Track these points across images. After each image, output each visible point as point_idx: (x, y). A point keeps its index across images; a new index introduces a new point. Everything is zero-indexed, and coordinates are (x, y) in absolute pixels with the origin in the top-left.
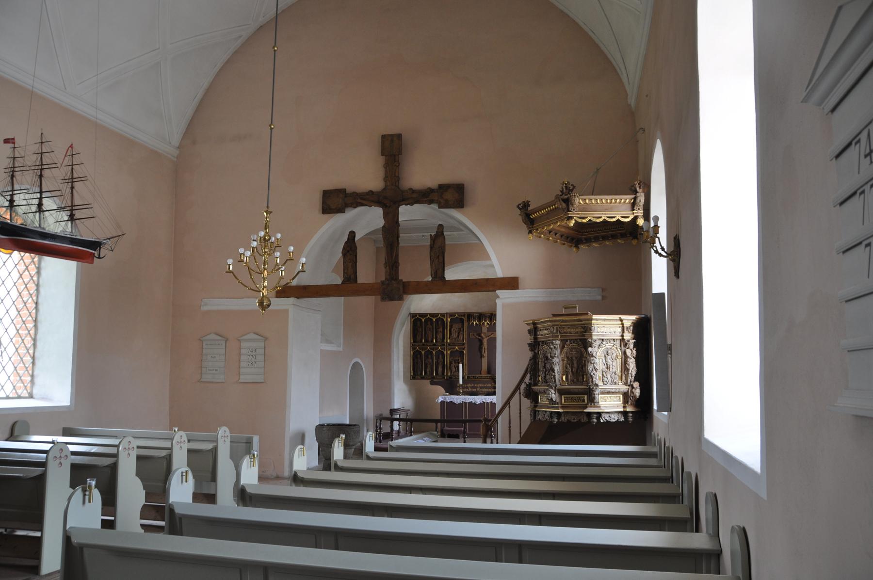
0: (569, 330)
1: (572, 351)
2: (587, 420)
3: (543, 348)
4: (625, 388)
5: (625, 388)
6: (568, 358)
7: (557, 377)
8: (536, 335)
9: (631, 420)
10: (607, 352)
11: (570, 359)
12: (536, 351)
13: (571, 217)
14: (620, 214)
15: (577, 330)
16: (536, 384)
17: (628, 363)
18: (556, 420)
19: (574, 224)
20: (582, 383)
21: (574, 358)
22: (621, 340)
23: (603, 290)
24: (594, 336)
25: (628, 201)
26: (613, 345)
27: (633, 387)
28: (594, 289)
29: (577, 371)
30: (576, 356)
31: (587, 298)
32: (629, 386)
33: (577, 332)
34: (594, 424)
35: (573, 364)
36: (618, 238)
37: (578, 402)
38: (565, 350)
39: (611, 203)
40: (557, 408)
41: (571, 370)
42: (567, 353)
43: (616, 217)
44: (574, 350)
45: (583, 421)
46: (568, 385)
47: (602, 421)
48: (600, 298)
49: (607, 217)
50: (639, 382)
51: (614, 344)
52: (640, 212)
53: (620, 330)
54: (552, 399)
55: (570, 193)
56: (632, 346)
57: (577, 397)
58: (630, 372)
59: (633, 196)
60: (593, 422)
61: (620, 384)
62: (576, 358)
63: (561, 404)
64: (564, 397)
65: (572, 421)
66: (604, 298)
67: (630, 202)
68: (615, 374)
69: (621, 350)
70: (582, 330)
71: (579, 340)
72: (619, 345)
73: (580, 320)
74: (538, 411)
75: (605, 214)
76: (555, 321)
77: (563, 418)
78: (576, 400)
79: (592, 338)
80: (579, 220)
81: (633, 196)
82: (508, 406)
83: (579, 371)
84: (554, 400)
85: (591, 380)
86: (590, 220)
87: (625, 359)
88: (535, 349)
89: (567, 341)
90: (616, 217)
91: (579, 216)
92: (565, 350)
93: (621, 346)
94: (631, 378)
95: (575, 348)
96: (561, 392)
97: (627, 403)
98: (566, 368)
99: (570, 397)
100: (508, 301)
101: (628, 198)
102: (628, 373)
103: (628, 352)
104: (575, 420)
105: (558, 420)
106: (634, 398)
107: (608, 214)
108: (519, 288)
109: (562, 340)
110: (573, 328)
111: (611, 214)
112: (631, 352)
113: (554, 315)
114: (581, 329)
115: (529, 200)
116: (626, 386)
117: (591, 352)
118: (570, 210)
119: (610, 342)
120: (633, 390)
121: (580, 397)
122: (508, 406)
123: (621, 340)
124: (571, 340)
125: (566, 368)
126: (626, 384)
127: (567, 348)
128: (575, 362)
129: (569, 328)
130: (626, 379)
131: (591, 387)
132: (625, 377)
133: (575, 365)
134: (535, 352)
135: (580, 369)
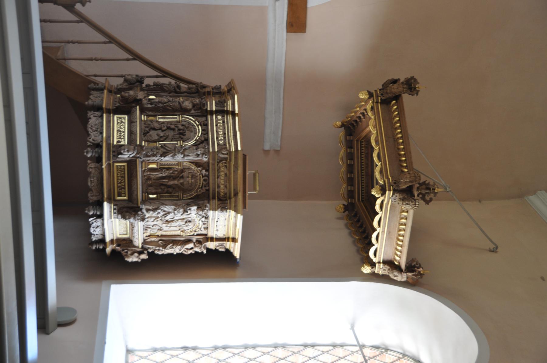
0: (222, 175)
1: (192, 177)
2: (91, 201)
3: (198, 126)
4: (138, 242)
5: (138, 242)
6: (182, 171)
7: (155, 158)
8: (215, 94)
9: (94, 247)
10: (190, 221)
11: (180, 173)
12: (193, 111)
13: (385, 193)
14: (381, 248)
15: (222, 186)
16: (142, 111)
17: (174, 247)
18: (89, 155)
19: (374, 196)
20: (146, 192)
21: (182, 181)
22: (206, 235)
23: (277, 151)
24: (213, 213)
25: (398, 258)
26: (200, 227)
27: (140, 253)
28: (279, 140)
29: (163, 185)
30: (185, 183)
31: (267, 131)
32: (142, 247)
33: (219, 187)
34: (86, 212)
35: (174, 179)
36: (348, 186)
37: (118, 187)
38: (193, 167)
39: (398, 240)
40: (108, 159)
41: (164, 175)
42: (189, 169)
43: (377, 243)
44: (193, 180)
45: (89, 195)
46: (144, 172)
47: (90, 219)
48: (267, 147)
49: (378, 233)
50: (148, 258)
51: (200, 229)
52: (380, 269)
53: (220, 234)
54: (121, 154)
55: (421, 196)
56: (197, 250)
57: (125, 185)
58: (161, 248)
59: (403, 266)
60: (89, 211)
61: (145, 235)
62: (182, 184)
63: (114, 162)
64: (124, 166)
65: (89, 180)
66: (266, 152)
67: (396, 260)
68: (159, 229)
69: (193, 235)
70: (222, 194)
71: (207, 188)
72: (200, 232)
73: (236, 194)
74: (102, 116)
75: (383, 232)
76: (236, 158)
77: (93, 165)
78: (120, 183)
79: (210, 210)
80: (378, 202)
81: (403, 266)
82: (107, 40)
83: (163, 187)
84: (120, 156)
85: (151, 208)
86: (375, 230)
87: (179, 241)
88: (195, 110)
89: (207, 170)
90: (377, 243)
91: (385, 202)
92: (193, 168)
93: (198, 235)
94: (151, 248)
95: (196, 182)
96: (132, 163)
97: (119, 245)
98: (168, 169)
99: (124, 174)
100: (270, 15)
101: (403, 262)
102: (159, 246)
103: (191, 245)
104: (91, 183)
105: (90, 158)
106: (125, 254)
107: (383, 234)
108: (289, 34)
109: (208, 163)
110: (226, 181)
111: (383, 238)
112: (188, 249)
113: (245, 156)
114: (224, 192)
115: (419, 93)
116: (142, 243)
117: (190, 209)
118: (396, 194)
119: (204, 224)
120: (136, 255)
121: (124, 188)
122: (107, 40)
123: (206, 235)
124: (208, 176)
125: (168, 169)
126: (145, 242)
127: (197, 170)
128: (176, 182)
129: (226, 174)
130: (151, 242)
131: (140, 213)
132: (154, 241)
133: (171, 183)
134: (190, 110)
135: (166, 189)
